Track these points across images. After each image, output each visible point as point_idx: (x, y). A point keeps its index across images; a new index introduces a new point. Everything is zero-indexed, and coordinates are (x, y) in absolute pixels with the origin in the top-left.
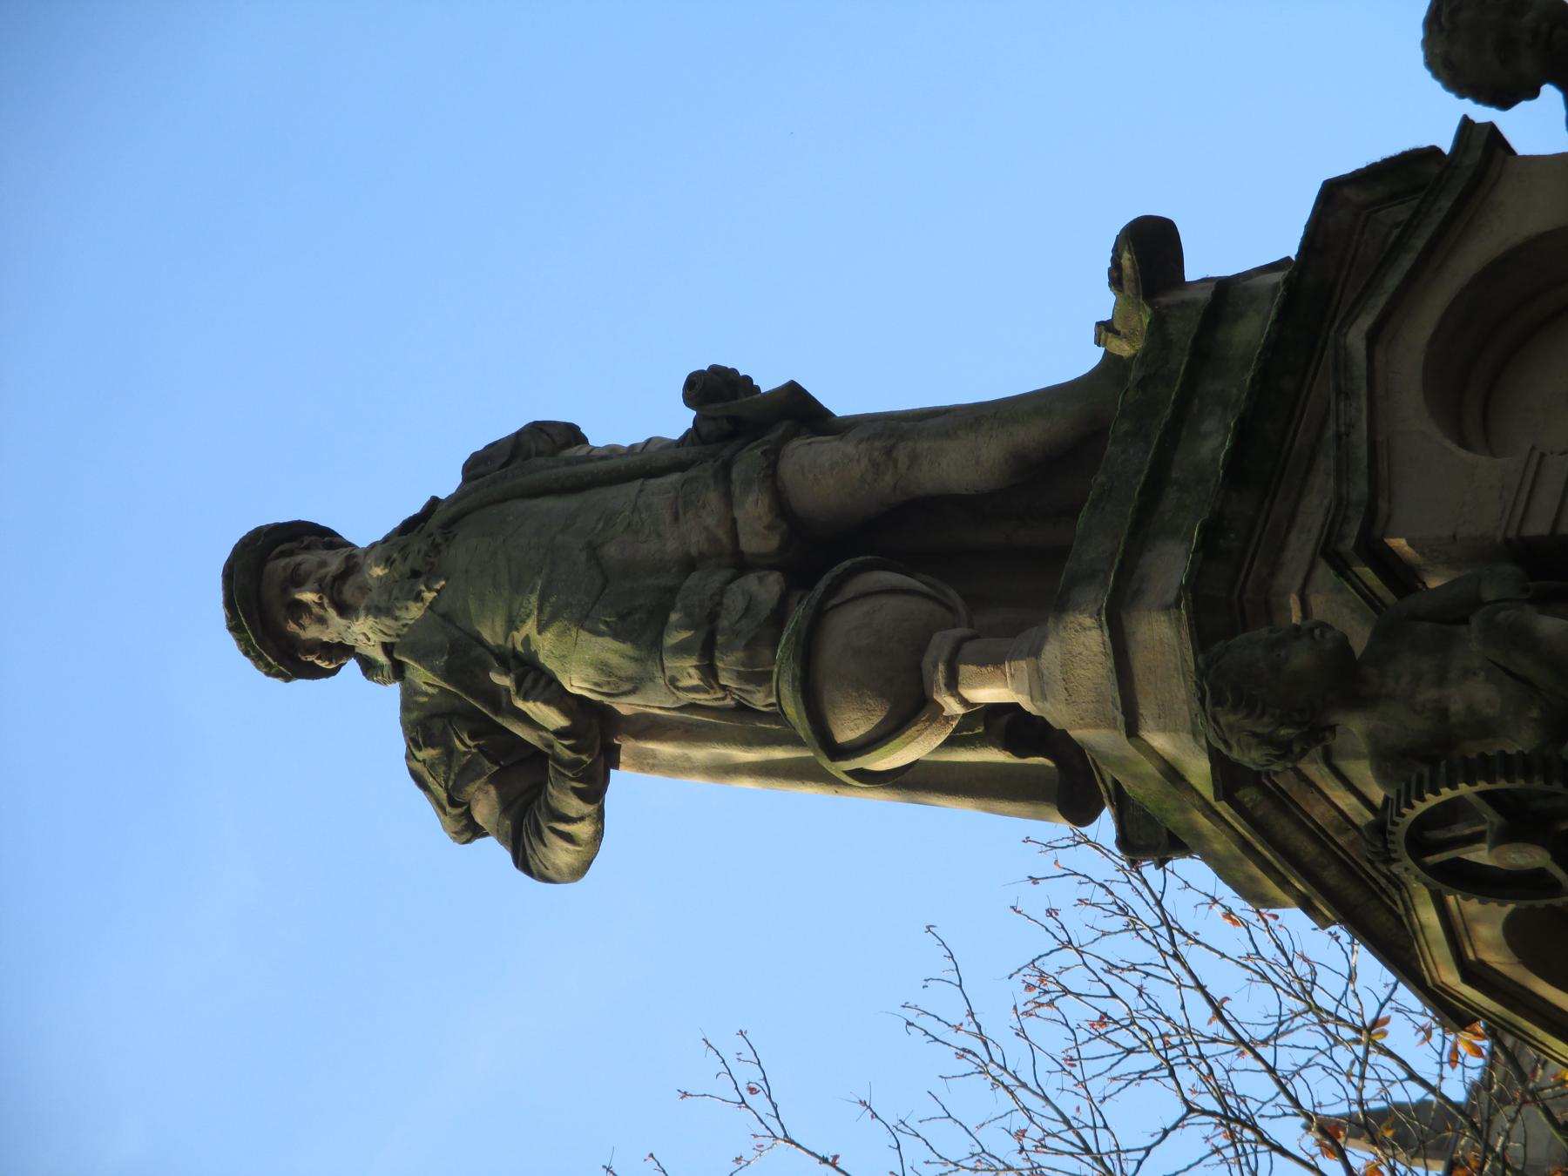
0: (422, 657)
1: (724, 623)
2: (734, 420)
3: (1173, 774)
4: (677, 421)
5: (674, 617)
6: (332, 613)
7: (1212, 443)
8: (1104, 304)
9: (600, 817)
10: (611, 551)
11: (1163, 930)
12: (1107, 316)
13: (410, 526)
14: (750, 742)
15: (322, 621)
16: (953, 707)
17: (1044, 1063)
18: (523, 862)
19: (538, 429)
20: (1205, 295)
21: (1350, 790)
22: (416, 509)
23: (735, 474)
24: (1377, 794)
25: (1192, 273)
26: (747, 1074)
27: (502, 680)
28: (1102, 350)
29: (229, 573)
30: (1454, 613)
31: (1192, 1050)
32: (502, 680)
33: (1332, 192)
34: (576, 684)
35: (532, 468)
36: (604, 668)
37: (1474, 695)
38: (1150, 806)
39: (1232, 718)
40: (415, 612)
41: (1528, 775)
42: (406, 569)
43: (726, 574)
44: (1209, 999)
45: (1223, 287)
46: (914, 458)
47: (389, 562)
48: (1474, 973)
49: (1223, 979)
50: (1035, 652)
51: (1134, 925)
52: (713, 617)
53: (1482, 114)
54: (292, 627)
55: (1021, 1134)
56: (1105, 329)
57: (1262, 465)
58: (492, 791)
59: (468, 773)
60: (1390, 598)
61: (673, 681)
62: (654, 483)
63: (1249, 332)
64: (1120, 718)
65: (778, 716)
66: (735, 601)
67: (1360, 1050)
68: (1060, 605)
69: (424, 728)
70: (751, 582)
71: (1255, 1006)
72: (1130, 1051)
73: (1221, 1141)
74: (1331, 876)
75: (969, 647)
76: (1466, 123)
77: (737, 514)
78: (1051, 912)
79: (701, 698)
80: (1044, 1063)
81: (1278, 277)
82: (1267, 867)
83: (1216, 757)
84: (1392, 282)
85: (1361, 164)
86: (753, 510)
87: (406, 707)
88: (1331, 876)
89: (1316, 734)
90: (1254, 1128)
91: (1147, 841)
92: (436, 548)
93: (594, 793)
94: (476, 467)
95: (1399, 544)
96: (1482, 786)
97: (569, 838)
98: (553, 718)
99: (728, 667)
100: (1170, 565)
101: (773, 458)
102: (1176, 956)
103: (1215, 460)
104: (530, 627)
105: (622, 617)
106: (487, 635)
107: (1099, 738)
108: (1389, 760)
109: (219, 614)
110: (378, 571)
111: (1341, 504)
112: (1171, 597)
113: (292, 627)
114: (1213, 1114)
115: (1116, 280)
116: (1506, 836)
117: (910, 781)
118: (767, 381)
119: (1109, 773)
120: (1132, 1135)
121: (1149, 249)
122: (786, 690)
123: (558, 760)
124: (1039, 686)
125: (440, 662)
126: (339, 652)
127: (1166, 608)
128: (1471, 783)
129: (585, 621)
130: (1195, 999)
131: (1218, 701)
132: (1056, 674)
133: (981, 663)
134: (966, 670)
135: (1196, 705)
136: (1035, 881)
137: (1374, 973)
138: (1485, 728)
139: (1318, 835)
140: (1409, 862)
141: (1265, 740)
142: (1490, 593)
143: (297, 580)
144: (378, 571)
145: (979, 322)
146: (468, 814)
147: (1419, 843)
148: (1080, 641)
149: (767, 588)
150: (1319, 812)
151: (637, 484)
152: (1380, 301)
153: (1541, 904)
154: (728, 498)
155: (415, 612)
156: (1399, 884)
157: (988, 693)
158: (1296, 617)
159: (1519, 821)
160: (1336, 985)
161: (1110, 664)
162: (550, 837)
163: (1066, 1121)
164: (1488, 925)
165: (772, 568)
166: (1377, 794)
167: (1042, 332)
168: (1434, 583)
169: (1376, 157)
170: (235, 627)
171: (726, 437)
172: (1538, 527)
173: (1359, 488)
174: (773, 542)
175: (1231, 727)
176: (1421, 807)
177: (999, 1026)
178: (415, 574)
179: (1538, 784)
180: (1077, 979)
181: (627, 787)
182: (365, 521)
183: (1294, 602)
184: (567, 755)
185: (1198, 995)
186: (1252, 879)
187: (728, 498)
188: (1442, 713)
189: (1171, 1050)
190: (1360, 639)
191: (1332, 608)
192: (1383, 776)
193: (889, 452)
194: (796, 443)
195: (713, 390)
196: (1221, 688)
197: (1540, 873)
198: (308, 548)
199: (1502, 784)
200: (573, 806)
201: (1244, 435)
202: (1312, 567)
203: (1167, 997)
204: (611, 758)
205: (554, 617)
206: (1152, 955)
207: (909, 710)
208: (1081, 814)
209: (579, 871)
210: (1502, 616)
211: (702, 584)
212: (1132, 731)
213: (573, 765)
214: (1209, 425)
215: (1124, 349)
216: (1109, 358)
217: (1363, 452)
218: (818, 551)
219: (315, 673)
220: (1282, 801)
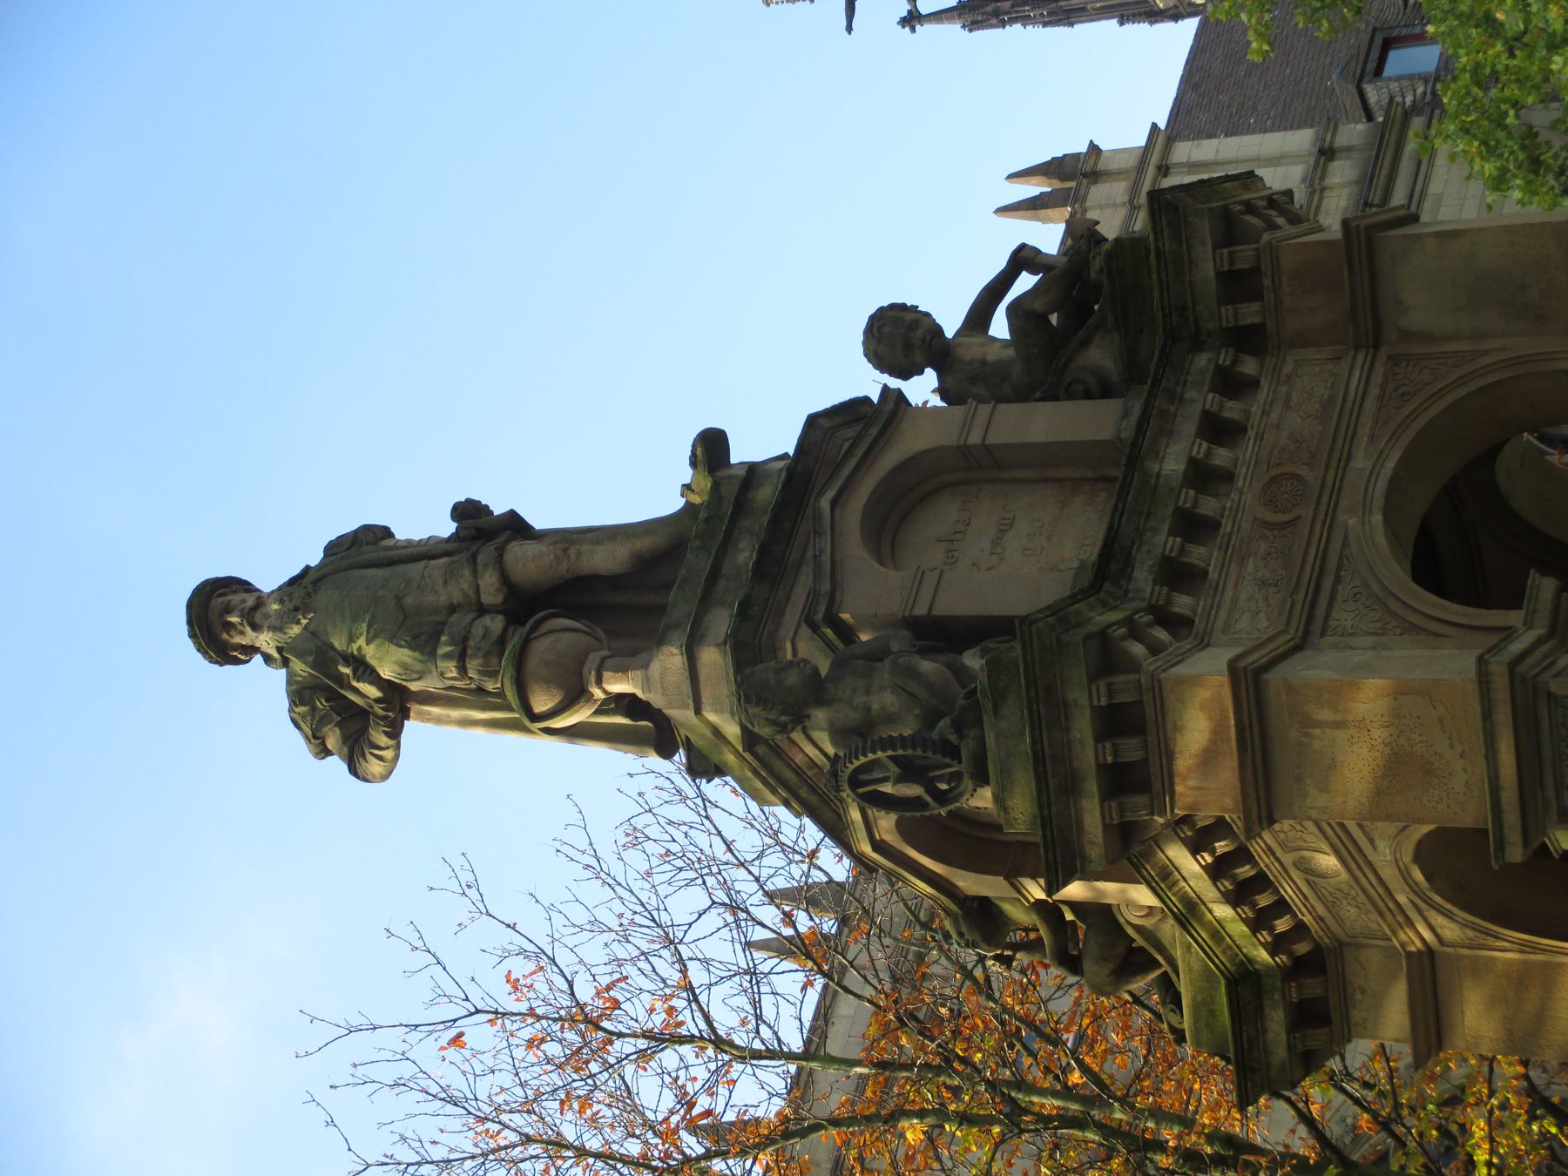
0: (300, 655)
1: (471, 643)
2: (477, 529)
3: (717, 732)
4: (447, 528)
5: (443, 638)
6: (248, 629)
7: (744, 555)
8: (687, 475)
9: (398, 747)
10: (409, 600)
11: (699, 801)
12: (688, 481)
13: (293, 581)
14: (484, 708)
15: (242, 633)
16: (598, 694)
17: (632, 875)
18: (354, 771)
19: (367, 529)
20: (742, 472)
21: (816, 745)
22: (296, 571)
23: (480, 559)
24: (831, 751)
25: (734, 459)
26: (466, 877)
27: (346, 670)
28: (683, 500)
29: (190, 606)
30: (877, 654)
31: (715, 869)
32: (346, 670)
33: (812, 421)
34: (386, 673)
35: (363, 552)
36: (405, 666)
37: (885, 700)
38: (705, 750)
39: (755, 710)
40: (295, 630)
41: (914, 748)
42: (291, 606)
43: (474, 615)
44: (725, 842)
45: (752, 468)
46: (579, 554)
47: (281, 601)
48: (878, 846)
49: (731, 828)
50: (646, 666)
51: (684, 799)
52: (465, 639)
53: (895, 383)
54: (225, 636)
55: (621, 916)
56: (687, 488)
57: (772, 568)
58: (337, 731)
59: (324, 720)
60: (840, 646)
61: (442, 674)
62: (433, 563)
63: (766, 494)
64: (691, 702)
65: (500, 694)
66: (478, 631)
67: (805, 867)
68: (661, 642)
69: (299, 695)
70: (487, 620)
71: (749, 843)
72: (681, 869)
73: (730, 919)
74: (804, 792)
75: (609, 662)
76: (885, 388)
77: (481, 582)
78: (640, 794)
79: (457, 684)
80: (632, 875)
81: (781, 464)
82: (765, 782)
83: (743, 728)
84: (845, 472)
85: (828, 405)
86: (489, 582)
87: (289, 683)
88: (804, 792)
89: (799, 719)
90: (747, 912)
91: (702, 767)
92: (309, 595)
93: (395, 733)
94: (332, 549)
95: (845, 616)
96: (890, 753)
97: (380, 758)
98: (373, 692)
99: (473, 666)
100: (721, 621)
101: (501, 551)
102: (707, 817)
103: (747, 564)
104: (362, 641)
105: (414, 638)
106: (337, 645)
107: (682, 716)
108: (838, 734)
109: (184, 628)
110: (275, 607)
111: (813, 595)
112: (721, 639)
113: (225, 636)
114: (724, 904)
115: (694, 463)
116: (901, 779)
117: (572, 733)
118: (498, 509)
119: (683, 732)
120: (681, 917)
121: (711, 446)
122: (507, 683)
123: (376, 715)
124: (647, 684)
125: (310, 659)
126: (251, 650)
127: (718, 645)
128: (884, 750)
129: (393, 639)
130: (717, 840)
131: (748, 701)
132: (657, 677)
133: (616, 671)
134: (606, 675)
135: (735, 699)
136: (631, 775)
137: (813, 833)
138: (891, 719)
139: (798, 771)
140: (848, 790)
141: (773, 722)
142: (895, 647)
143: (228, 610)
144: (275, 607)
145: (610, 477)
146: (323, 744)
147: (855, 783)
148: (670, 660)
149: (496, 624)
150: (799, 759)
151: (423, 563)
152: (838, 484)
153: (918, 814)
154: (475, 573)
155: (295, 630)
156: (841, 801)
157: (618, 687)
158: (789, 657)
159: (909, 771)
160: (793, 834)
161: (687, 674)
162: (369, 757)
163: (642, 904)
164: (886, 824)
165: (499, 612)
166: (831, 751)
167: (653, 488)
168: (864, 637)
169: (836, 402)
170: (192, 635)
171: (475, 539)
172: (920, 610)
173: (826, 586)
174: (499, 599)
175: (755, 715)
176: (857, 763)
177: (607, 852)
178: (297, 609)
179: (919, 752)
180: (654, 832)
181: (412, 729)
182: (268, 577)
183: (788, 645)
184: (381, 712)
185: (718, 839)
186: (757, 790)
187: (475, 573)
188: (868, 709)
189: (702, 868)
190: (824, 667)
191: (807, 650)
192: (834, 743)
193: (565, 551)
194: (513, 544)
195: (468, 512)
196: (750, 693)
197: (919, 798)
198: (235, 592)
199: (900, 752)
200: (383, 740)
201: (763, 553)
202: (798, 626)
203: (702, 839)
204: (405, 714)
205: (375, 637)
206: (697, 819)
207: (575, 695)
208: (666, 752)
209: (385, 777)
210: (901, 660)
211: (460, 620)
212: (698, 711)
213: (384, 718)
214: (743, 545)
215: (697, 500)
216: (688, 504)
217: (828, 567)
218: (526, 605)
219: (237, 662)
220: (777, 751)
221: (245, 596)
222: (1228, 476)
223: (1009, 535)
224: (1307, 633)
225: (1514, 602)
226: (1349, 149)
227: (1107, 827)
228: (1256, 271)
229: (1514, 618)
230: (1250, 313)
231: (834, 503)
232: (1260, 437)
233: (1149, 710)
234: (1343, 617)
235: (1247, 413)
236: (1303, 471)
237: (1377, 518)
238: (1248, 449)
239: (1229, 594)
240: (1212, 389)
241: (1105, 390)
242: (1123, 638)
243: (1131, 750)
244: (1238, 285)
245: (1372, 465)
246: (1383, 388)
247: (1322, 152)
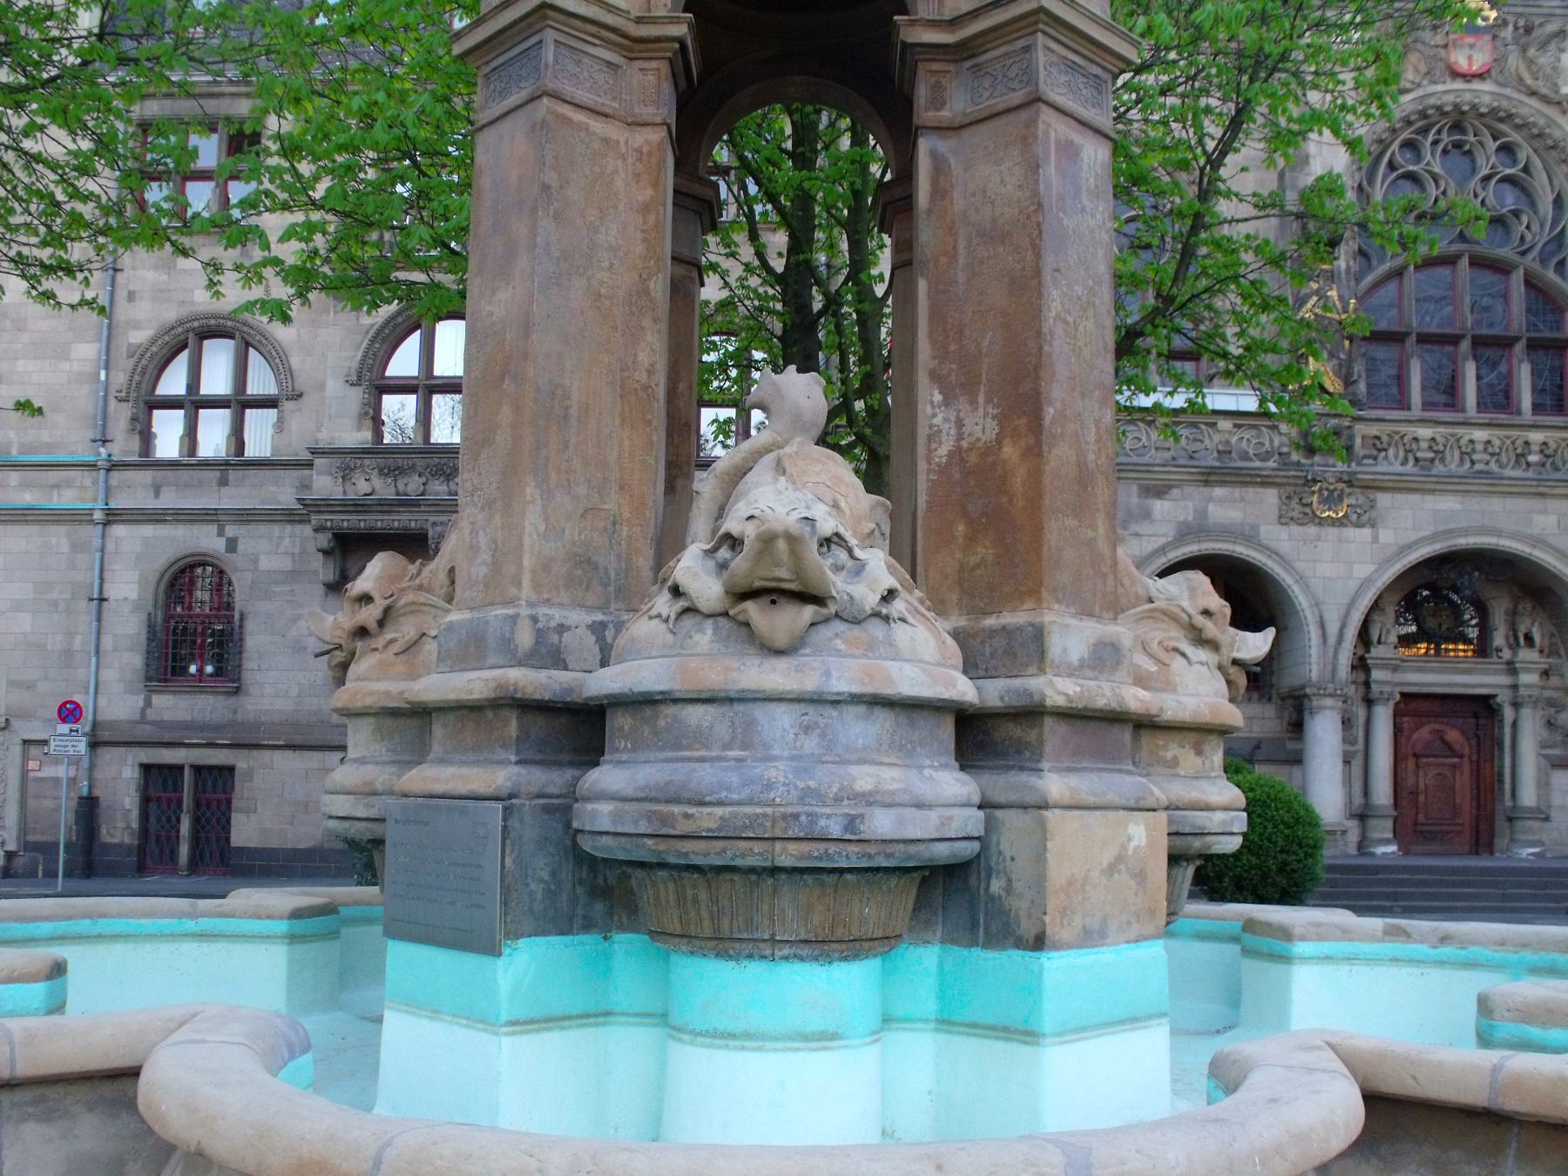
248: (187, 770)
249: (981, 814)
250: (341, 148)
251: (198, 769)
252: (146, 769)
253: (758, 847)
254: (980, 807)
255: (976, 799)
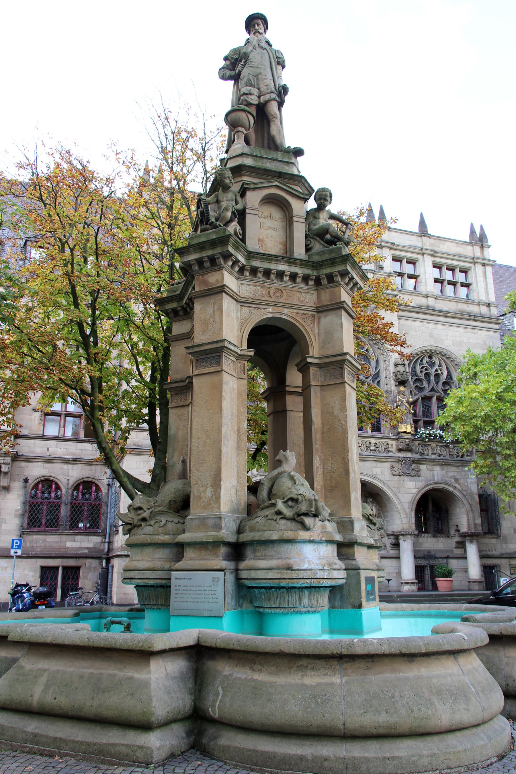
8: (292, 147)
145: (293, 127)
172: (247, 211)
174: (262, 101)
221: (263, 29)
222: (282, 280)
223: (272, 231)
224: (241, 302)
225: (249, 347)
226: (490, 310)
227: (189, 261)
228: (333, 282)
229: (245, 347)
230: (324, 282)
231: (276, 186)
232: (293, 287)
233: (216, 268)
234: (245, 310)
235: (299, 283)
236: (284, 297)
237: (271, 315)
238: (290, 284)
239: (251, 283)
240: (304, 275)
241: (308, 249)
242: (232, 260)
243: (207, 264)
244: (330, 278)
245: (286, 314)
246: (306, 314)
247: (489, 304)
248: (60, 570)
249: (346, 572)
250: (18, 347)
251: (65, 568)
252: (43, 568)
253: (308, 581)
254: (345, 570)
255: (344, 567)
